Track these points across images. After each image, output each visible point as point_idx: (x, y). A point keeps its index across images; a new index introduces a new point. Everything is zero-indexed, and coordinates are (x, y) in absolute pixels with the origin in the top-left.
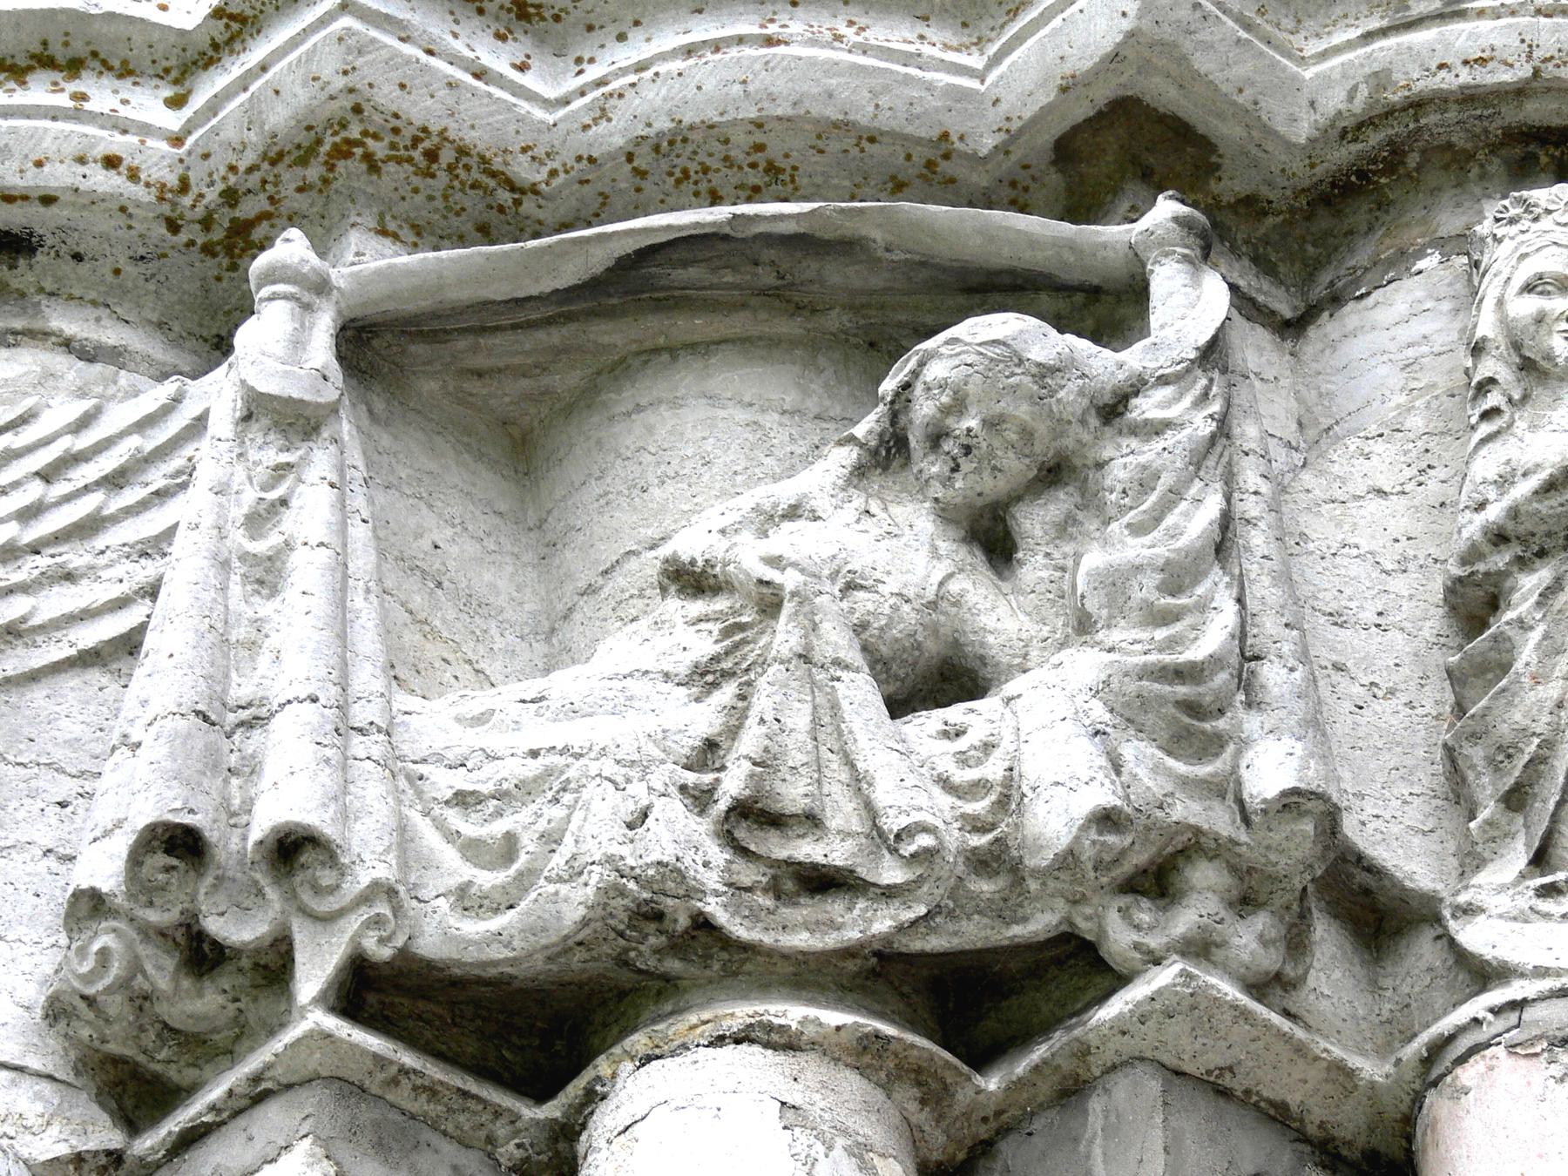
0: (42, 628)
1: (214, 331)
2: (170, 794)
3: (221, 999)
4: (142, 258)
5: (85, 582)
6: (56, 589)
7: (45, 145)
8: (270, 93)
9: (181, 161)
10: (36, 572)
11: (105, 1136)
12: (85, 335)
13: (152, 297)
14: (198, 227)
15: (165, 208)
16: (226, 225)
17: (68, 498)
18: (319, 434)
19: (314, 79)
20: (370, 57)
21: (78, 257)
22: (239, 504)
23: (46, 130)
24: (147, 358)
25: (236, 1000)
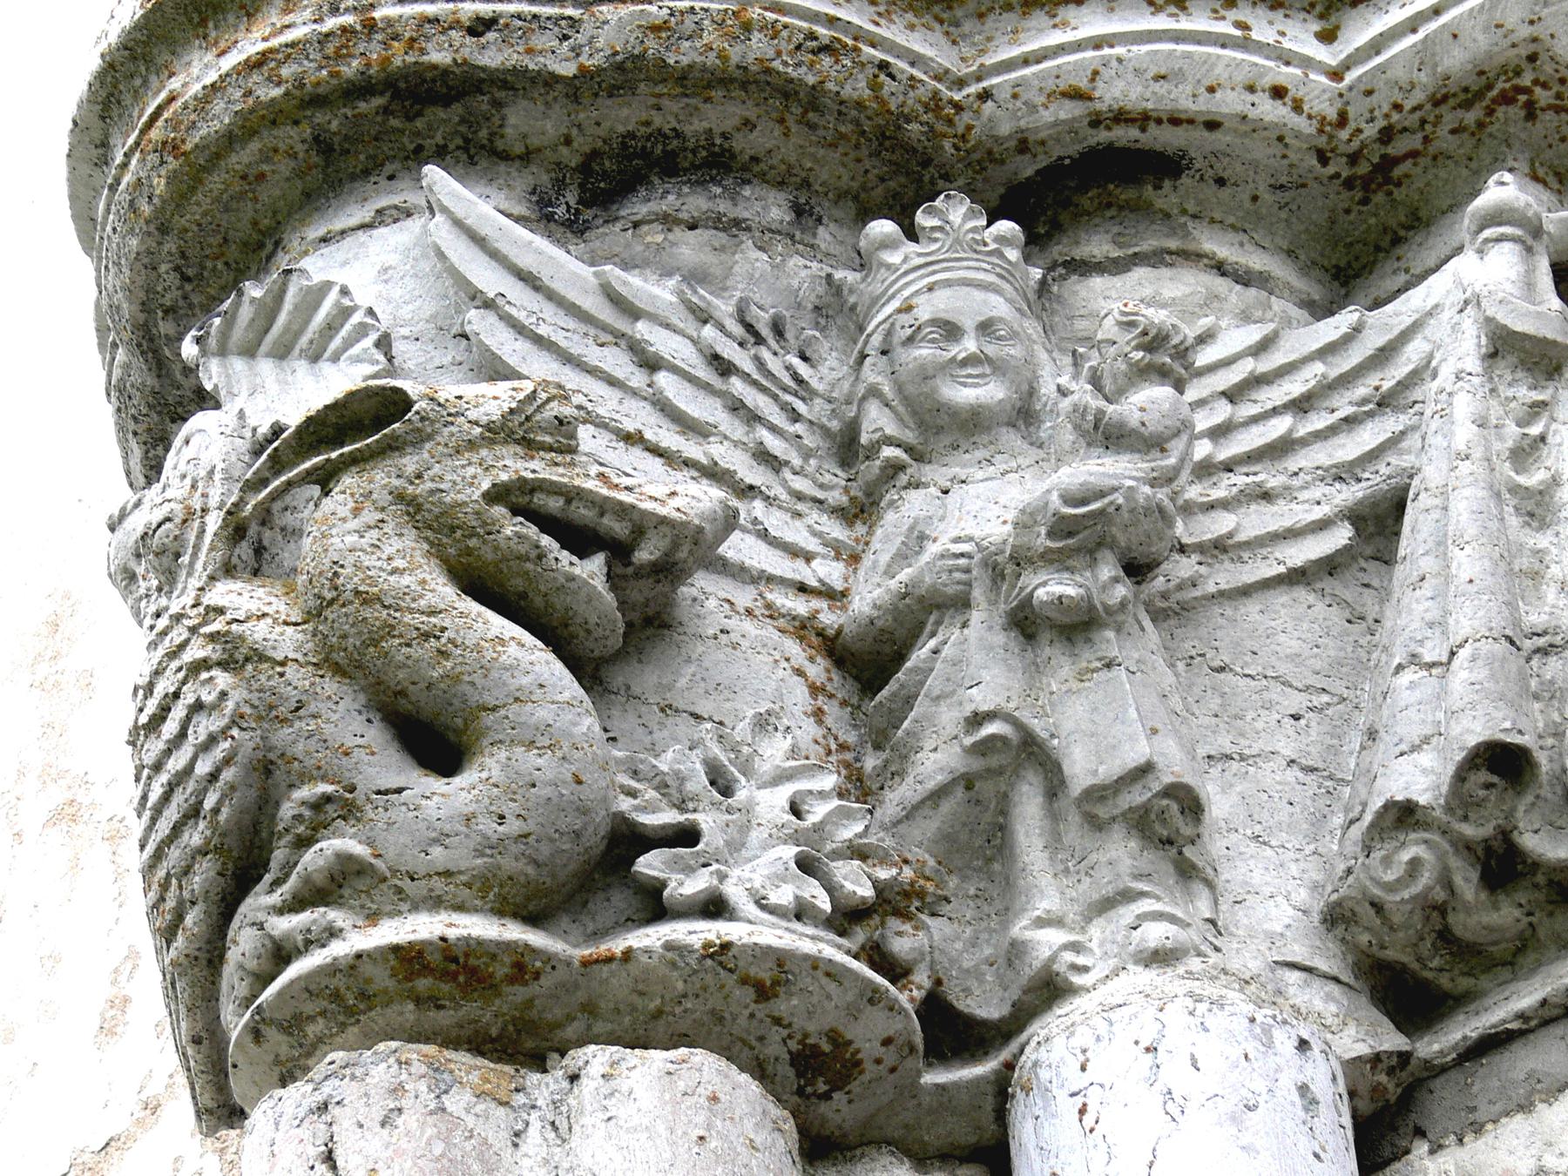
0: (1247, 545)
1: (1334, 262)
2: (1496, 714)
3: (1517, 913)
4: (1282, 186)
5: (1281, 502)
6: (1253, 507)
7: (1217, 71)
8: (1447, 36)
9: (1341, 95)
10: (1235, 490)
11: (1392, 1041)
12: (1234, 259)
13: (1283, 224)
14: (1344, 159)
15: (1322, 141)
16: (1376, 160)
17: (1255, 420)
18: (1560, 375)
19: (1497, 26)
20: (1554, 8)
21: (1221, 182)
22: (1501, 438)
23: (1219, 57)
24: (1292, 290)
25: (1529, 914)
